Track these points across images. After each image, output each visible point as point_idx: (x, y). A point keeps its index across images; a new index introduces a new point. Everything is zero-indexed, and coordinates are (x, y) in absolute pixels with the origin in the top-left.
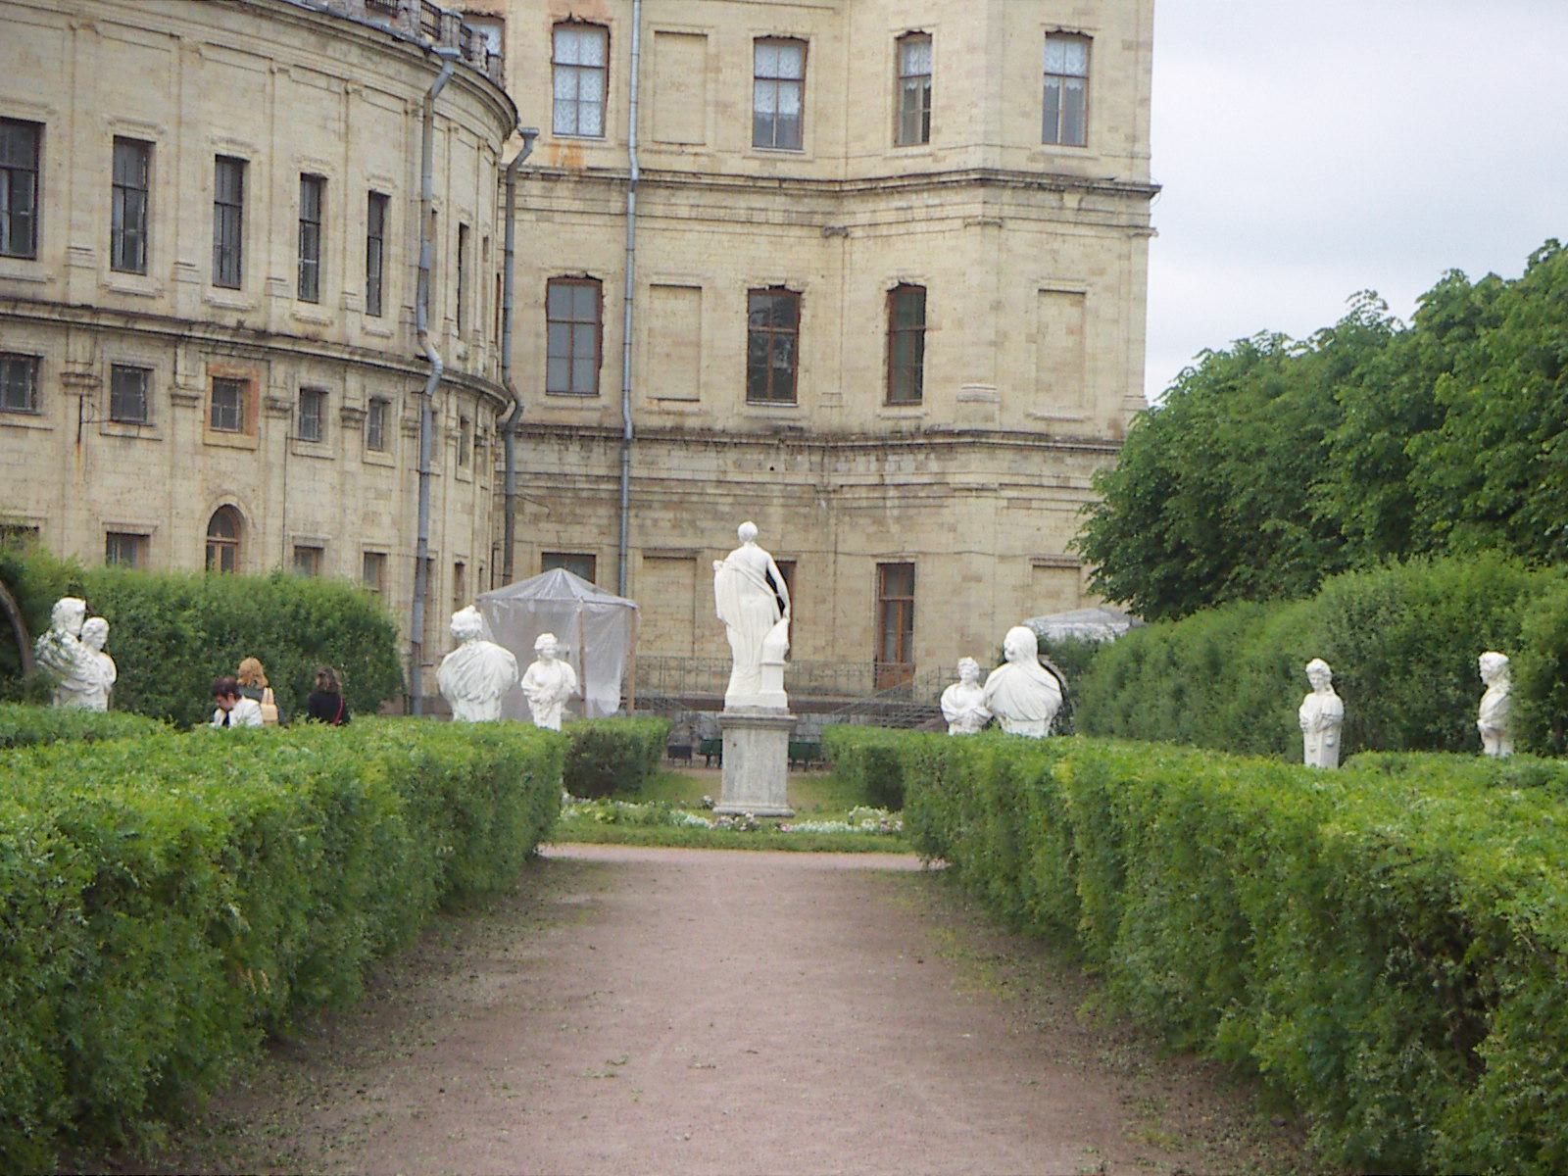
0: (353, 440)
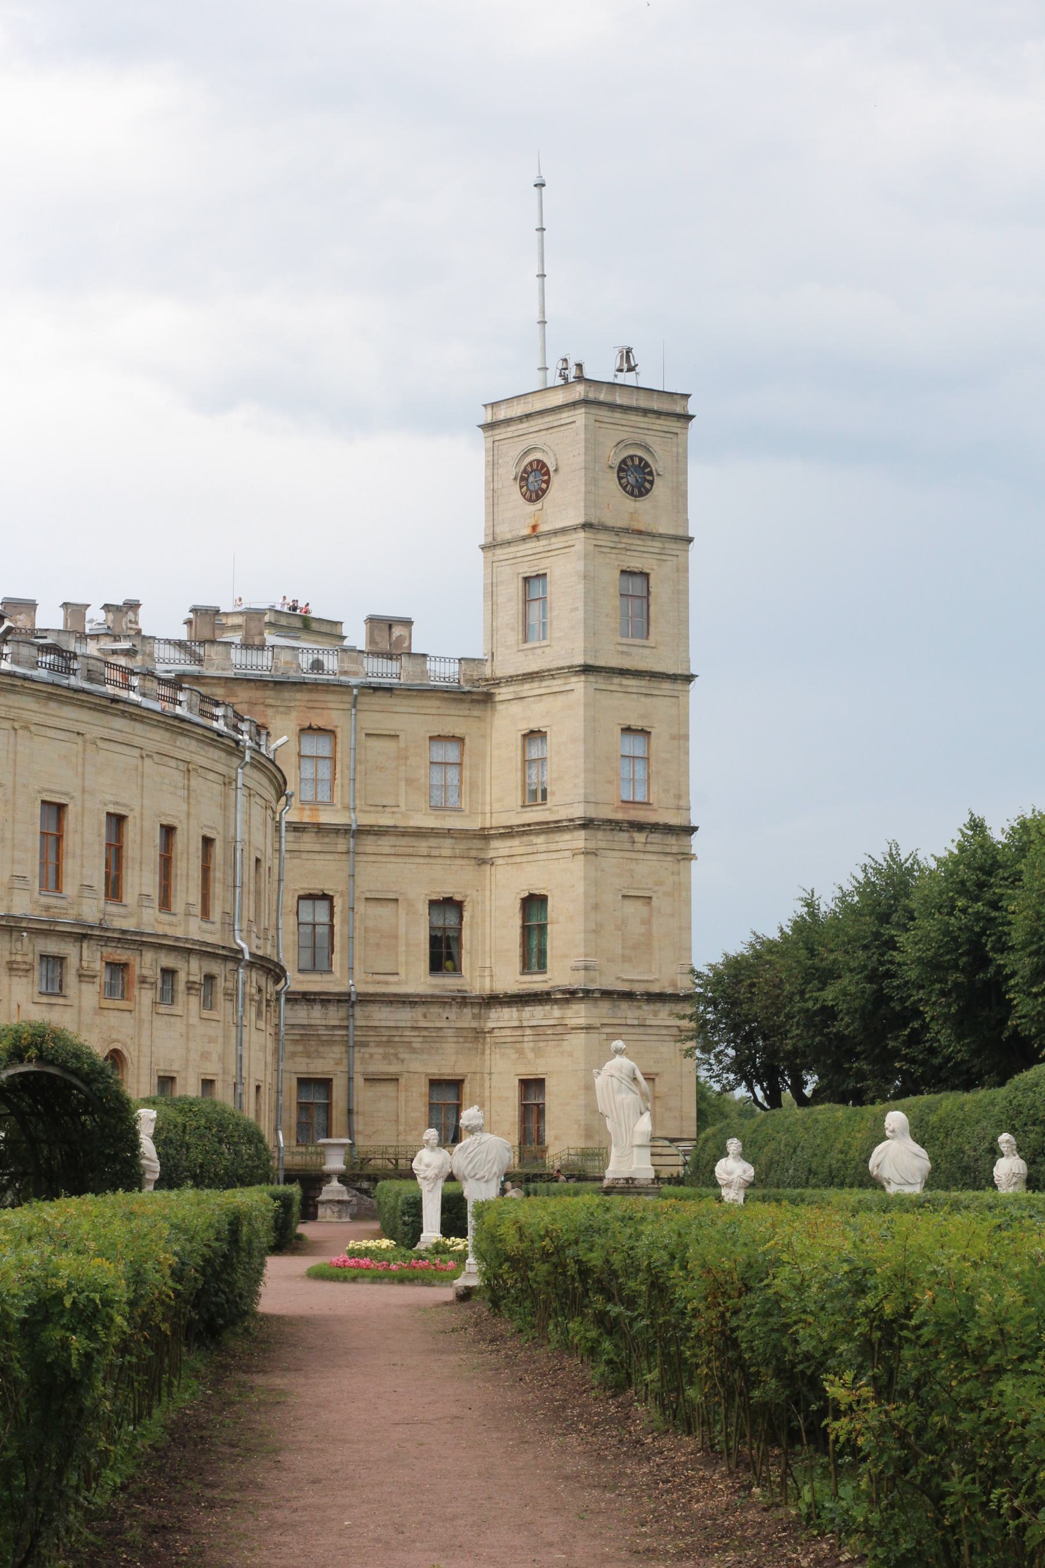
0: (194, 1002)
